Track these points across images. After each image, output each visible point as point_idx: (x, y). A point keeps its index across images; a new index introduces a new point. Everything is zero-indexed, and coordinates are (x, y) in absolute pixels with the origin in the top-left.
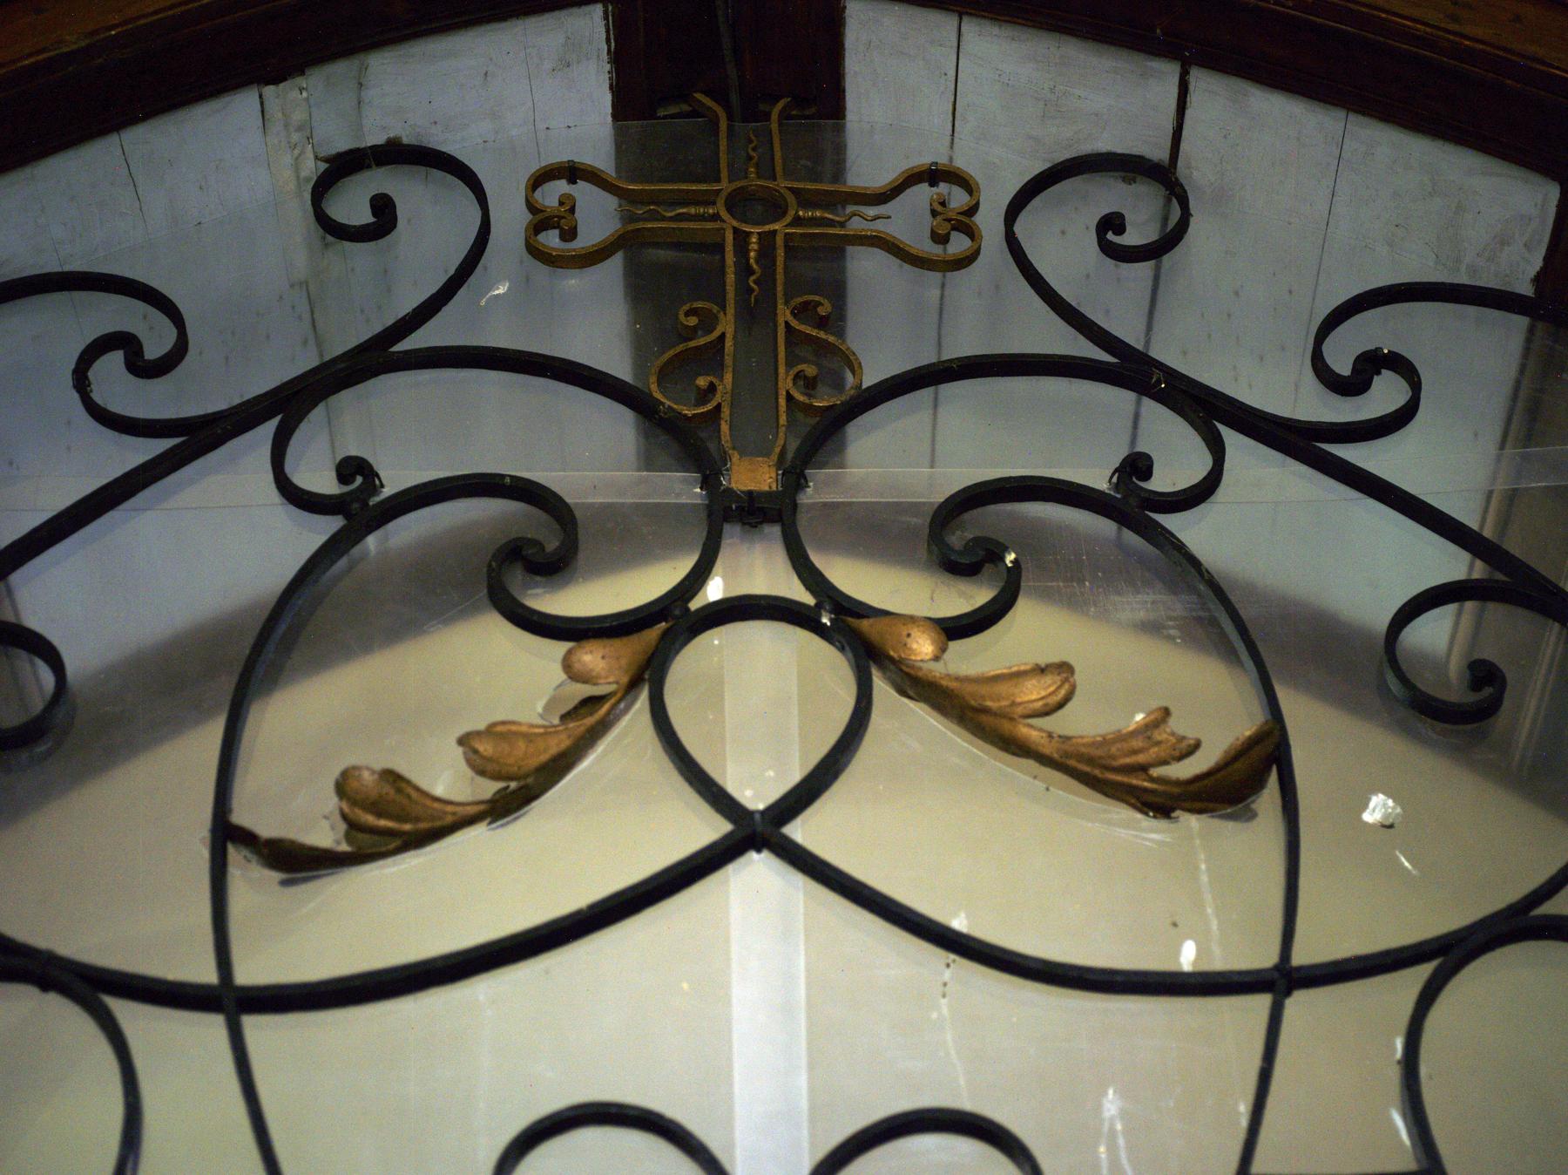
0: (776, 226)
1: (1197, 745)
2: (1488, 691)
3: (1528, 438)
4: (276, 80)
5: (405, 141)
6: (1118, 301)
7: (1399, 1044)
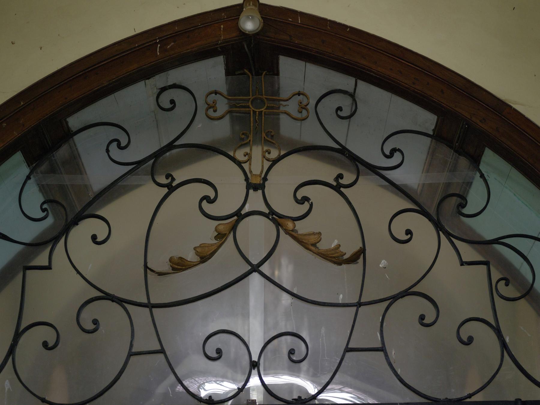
0: (262, 110)
1: (345, 254)
2: (409, 236)
3: (428, 171)
4: (148, 79)
5: (177, 83)
6: (339, 129)
7: (381, 318)
